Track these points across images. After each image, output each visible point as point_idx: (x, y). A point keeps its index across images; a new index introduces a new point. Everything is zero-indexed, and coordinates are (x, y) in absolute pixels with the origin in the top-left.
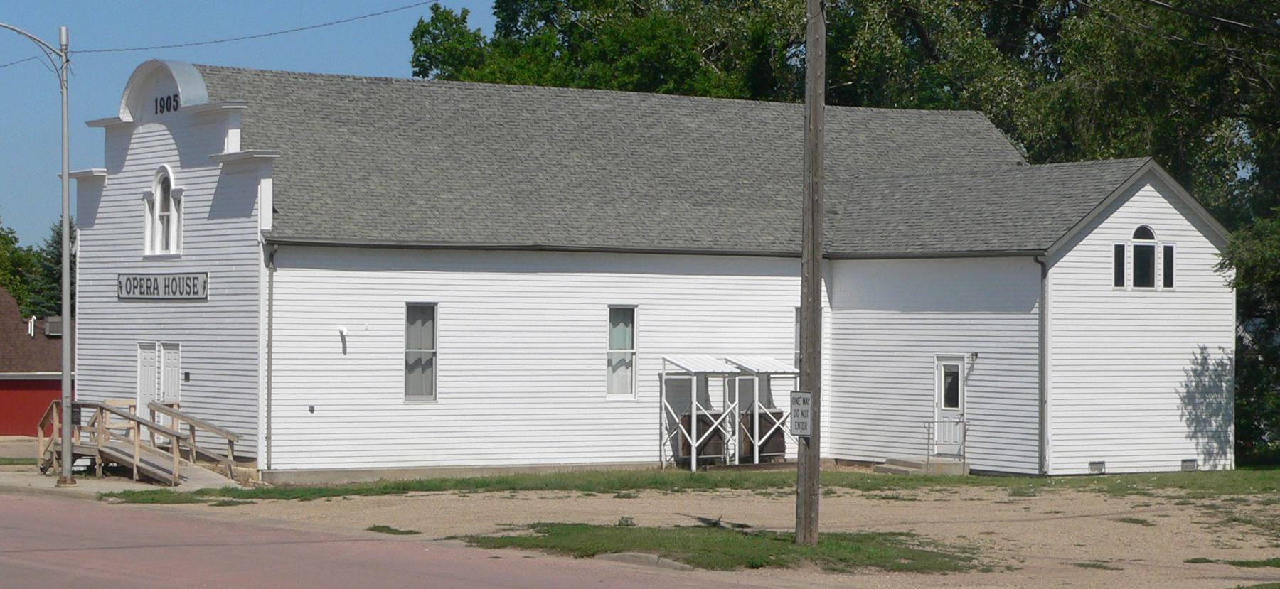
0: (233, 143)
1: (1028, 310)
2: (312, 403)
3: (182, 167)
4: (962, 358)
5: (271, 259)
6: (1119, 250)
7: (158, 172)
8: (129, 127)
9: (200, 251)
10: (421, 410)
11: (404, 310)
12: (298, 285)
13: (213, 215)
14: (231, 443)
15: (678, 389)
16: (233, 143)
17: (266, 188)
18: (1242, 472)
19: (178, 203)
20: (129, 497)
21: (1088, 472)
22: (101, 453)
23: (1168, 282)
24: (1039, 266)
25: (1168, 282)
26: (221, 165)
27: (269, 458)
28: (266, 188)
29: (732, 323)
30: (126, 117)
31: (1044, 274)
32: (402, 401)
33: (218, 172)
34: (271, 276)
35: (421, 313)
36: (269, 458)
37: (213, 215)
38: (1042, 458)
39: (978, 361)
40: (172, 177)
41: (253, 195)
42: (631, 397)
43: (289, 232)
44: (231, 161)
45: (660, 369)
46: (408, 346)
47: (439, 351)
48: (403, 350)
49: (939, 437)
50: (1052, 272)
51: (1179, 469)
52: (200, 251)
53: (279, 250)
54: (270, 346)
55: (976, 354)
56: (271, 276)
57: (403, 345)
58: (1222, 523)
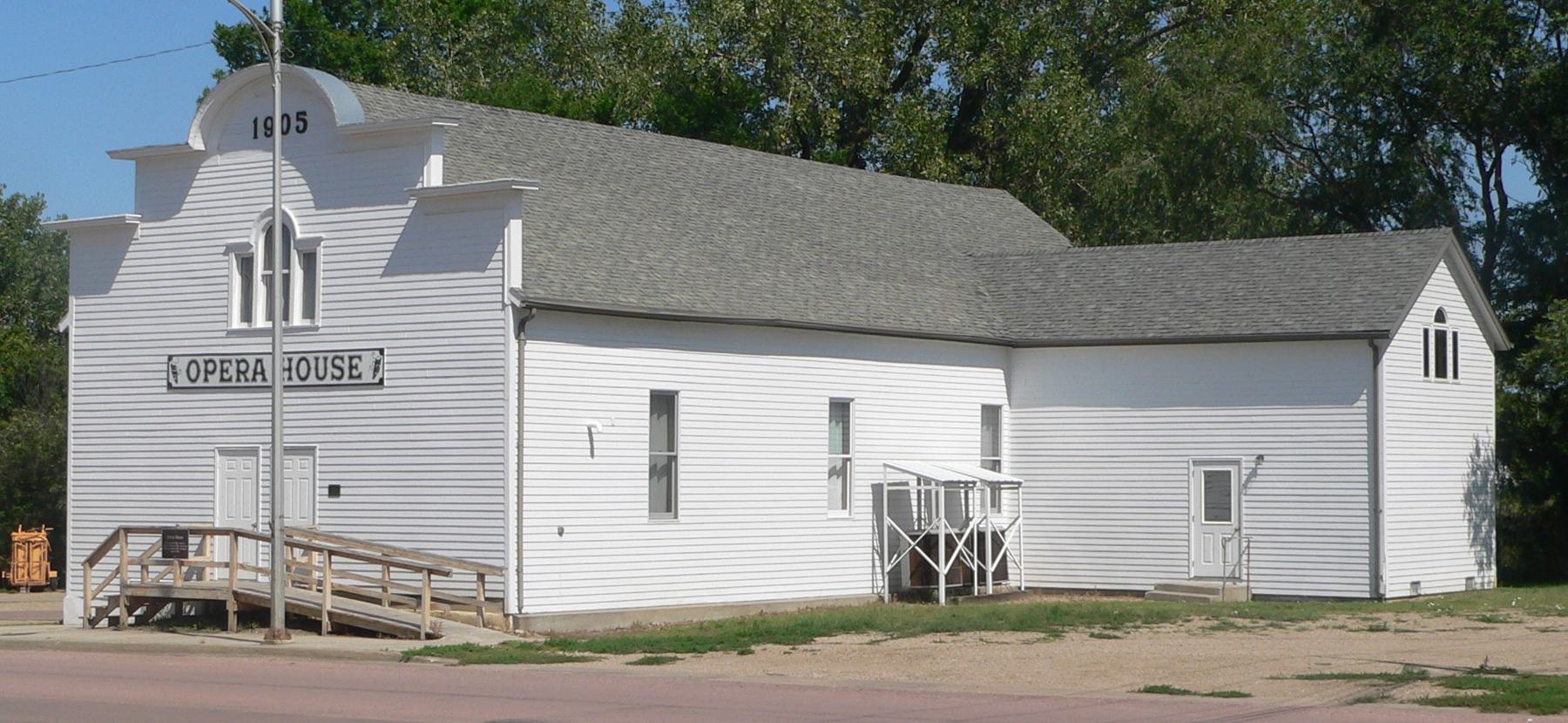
0: (434, 173)
1: (1349, 400)
2: (561, 523)
3: (317, 207)
4: (1237, 463)
5: (524, 324)
6: (1426, 332)
7: (262, 217)
8: (202, 156)
9: (183, 328)
10: (665, 529)
11: (648, 400)
12: (555, 363)
13: (390, 270)
14: (481, 577)
15: (890, 501)
16: (434, 173)
17: (515, 228)
18: (1510, 592)
19: (309, 260)
20: (407, 657)
21: (1408, 594)
22: (235, 593)
23: (1456, 376)
24: (1371, 351)
25: (1456, 376)
26: (412, 203)
27: (520, 599)
28: (515, 228)
29: (928, 418)
30: (197, 144)
31: (1377, 360)
32: (646, 520)
33: (408, 212)
34: (521, 351)
35: (664, 403)
36: (520, 599)
37: (390, 270)
38: (1376, 578)
39: (1264, 465)
40: (296, 221)
41: (498, 237)
42: (845, 514)
43: (541, 293)
44: (430, 201)
45: (878, 478)
46: (651, 449)
47: (681, 454)
48: (647, 453)
49: (1199, 555)
50: (1387, 359)
51: (1463, 588)
52: (183, 328)
53: (536, 316)
54: (520, 447)
55: (1260, 458)
56: (521, 351)
57: (647, 446)
58: (1213, 628)
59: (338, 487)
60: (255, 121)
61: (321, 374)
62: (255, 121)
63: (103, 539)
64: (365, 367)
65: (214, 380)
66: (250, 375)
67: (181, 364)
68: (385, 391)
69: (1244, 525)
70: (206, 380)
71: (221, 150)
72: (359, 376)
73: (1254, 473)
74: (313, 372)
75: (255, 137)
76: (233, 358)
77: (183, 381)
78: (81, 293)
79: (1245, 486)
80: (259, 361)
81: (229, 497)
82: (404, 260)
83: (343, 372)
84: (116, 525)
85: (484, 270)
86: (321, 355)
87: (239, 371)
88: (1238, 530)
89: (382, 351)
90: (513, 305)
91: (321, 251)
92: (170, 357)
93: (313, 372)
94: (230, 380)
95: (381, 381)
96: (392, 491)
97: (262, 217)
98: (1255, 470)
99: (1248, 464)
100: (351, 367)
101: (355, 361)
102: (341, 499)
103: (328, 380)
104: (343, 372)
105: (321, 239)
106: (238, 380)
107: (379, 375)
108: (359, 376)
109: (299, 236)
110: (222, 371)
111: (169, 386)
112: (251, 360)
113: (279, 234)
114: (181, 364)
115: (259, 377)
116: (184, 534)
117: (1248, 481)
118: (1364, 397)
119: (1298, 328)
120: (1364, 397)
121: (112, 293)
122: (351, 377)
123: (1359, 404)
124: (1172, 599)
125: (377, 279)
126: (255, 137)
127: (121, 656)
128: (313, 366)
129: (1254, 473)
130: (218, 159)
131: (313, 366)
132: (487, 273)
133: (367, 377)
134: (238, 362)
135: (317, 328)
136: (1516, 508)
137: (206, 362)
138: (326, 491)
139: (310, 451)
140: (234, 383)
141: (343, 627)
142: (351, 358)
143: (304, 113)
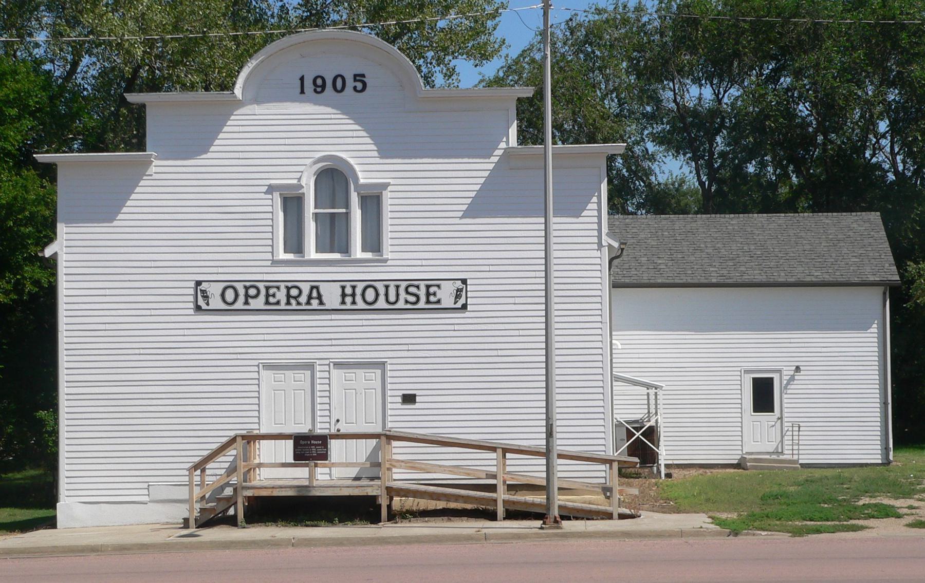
3: (381, 158)
4: (779, 371)
7: (315, 163)
8: (240, 104)
59: (414, 396)
60: (302, 79)
61: (392, 298)
62: (302, 79)
63: (215, 447)
64: (446, 295)
65: (258, 303)
66: (303, 299)
67: (215, 290)
68: (467, 314)
69: (786, 415)
70: (246, 303)
71: (257, 101)
72: (439, 302)
73: (792, 378)
74: (382, 298)
75: (302, 92)
76: (282, 285)
77: (216, 303)
78: (69, 221)
79: (786, 388)
80: (312, 288)
81: (350, 405)
82: (483, 205)
83: (420, 297)
84: (232, 434)
85: (578, 216)
86: (392, 284)
87: (289, 296)
88: (781, 418)
89: (464, 281)
90: (610, 246)
91: (387, 196)
92: (198, 283)
93: (382, 298)
94: (278, 303)
95: (464, 307)
96: (848, 391)
97: (315, 163)
98: (794, 375)
99: (788, 372)
100: (428, 294)
101: (432, 290)
102: (417, 406)
103: (401, 304)
104: (420, 297)
105: (388, 184)
106: (288, 303)
107: (462, 301)
108: (439, 302)
109: (362, 181)
110: (267, 296)
111: (198, 308)
112: (306, 288)
113: (334, 178)
114: (215, 290)
115: (349, 300)
116: (324, 440)
117: (788, 384)
118: (875, 326)
119: (827, 278)
120: (875, 326)
121: (115, 223)
122: (428, 302)
123: (872, 330)
124: (762, 468)
125: (457, 221)
126: (302, 92)
127: (659, 541)
128: (382, 291)
129: (792, 378)
130: (256, 109)
131: (382, 291)
132: (581, 220)
133: (448, 302)
134: (288, 289)
135: (386, 260)
136: (42, 414)
137: (247, 288)
138: (400, 400)
139: (382, 365)
140: (283, 306)
141: (513, 514)
142: (428, 287)
143: (363, 76)
